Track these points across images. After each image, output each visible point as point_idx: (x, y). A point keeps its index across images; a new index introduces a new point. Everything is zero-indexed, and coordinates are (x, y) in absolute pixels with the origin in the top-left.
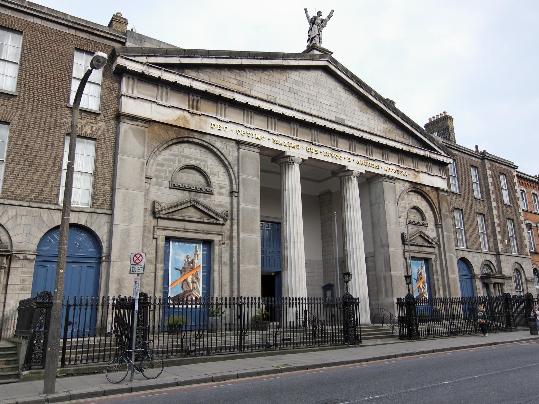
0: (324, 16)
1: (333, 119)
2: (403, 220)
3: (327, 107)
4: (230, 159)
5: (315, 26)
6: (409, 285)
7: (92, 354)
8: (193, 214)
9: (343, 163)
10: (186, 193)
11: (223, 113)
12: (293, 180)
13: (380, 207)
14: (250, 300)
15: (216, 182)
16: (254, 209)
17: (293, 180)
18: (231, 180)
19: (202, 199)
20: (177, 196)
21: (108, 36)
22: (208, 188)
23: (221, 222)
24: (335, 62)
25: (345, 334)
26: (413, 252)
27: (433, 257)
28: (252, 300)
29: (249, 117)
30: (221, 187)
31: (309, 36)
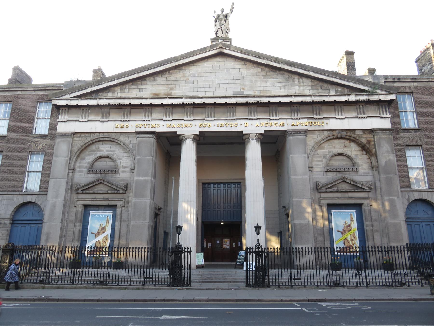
6: (258, 235)
8: (344, 187)
9: (238, 129)
10: (335, 173)
12: (189, 153)
16: (146, 180)
17: (189, 153)
19: (348, 175)
20: (331, 176)
21: (54, 88)
23: (368, 190)
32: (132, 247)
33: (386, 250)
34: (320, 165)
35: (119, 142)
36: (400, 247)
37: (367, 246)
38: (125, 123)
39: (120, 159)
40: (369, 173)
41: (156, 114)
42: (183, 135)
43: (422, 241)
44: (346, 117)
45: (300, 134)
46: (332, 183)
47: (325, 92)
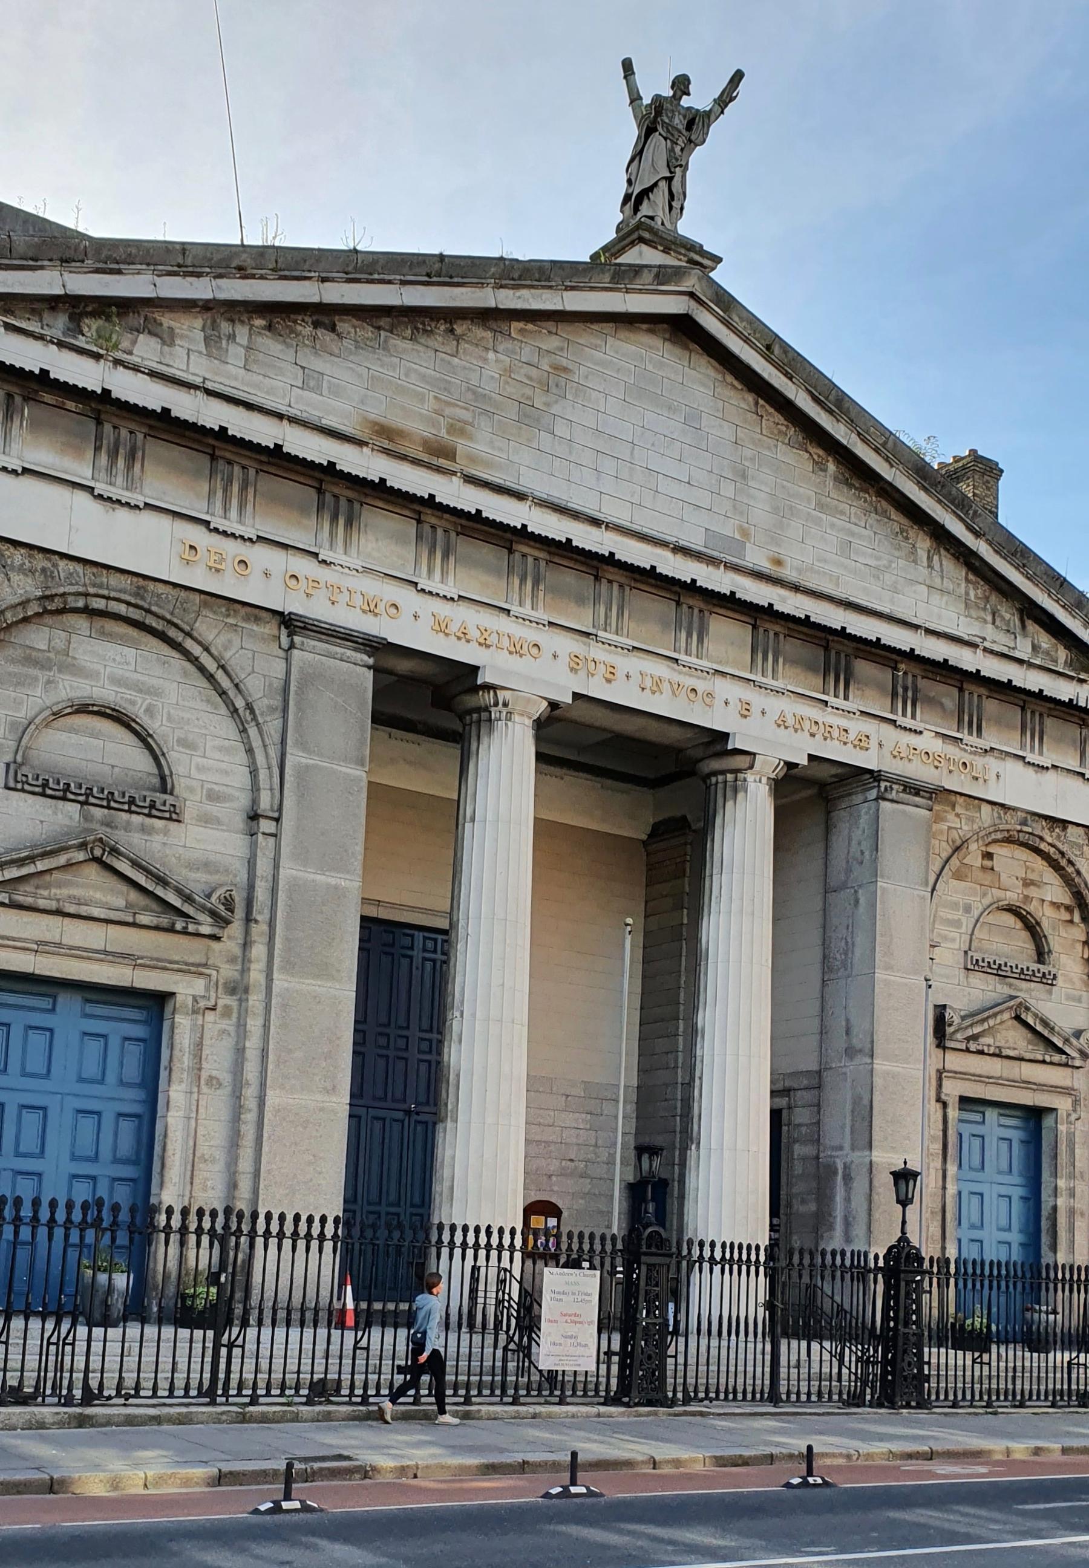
0: (699, 99)
1: (696, 542)
2: (949, 956)
3: (675, 490)
4: (255, 687)
5: (656, 139)
7: (478, 1378)
8: (96, 890)
11: (235, 502)
13: (857, 901)
14: (317, 1224)
15: (194, 773)
16: (336, 887)
18: (254, 773)
22: (159, 797)
23: (206, 930)
24: (725, 302)
25: (884, 1373)
26: (979, 1078)
27: (1062, 1104)
28: (581, 1243)
29: (341, 521)
30: (213, 797)
31: (630, 182)
32: (829, 1249)
33: (718, 1256)
34: (953, 940)
35: (196, 650)
36: (282, 1217)
37: (1044, 1262)
38: (232, 548)
39: (183, 743)
40: (1079, 1000)
41: (382, 541)
42: (501, 695)
43: (233, 1186)
44: (1054, 767)
45: (917, 799)
46: (31, 859)
47: (1000, 640)
